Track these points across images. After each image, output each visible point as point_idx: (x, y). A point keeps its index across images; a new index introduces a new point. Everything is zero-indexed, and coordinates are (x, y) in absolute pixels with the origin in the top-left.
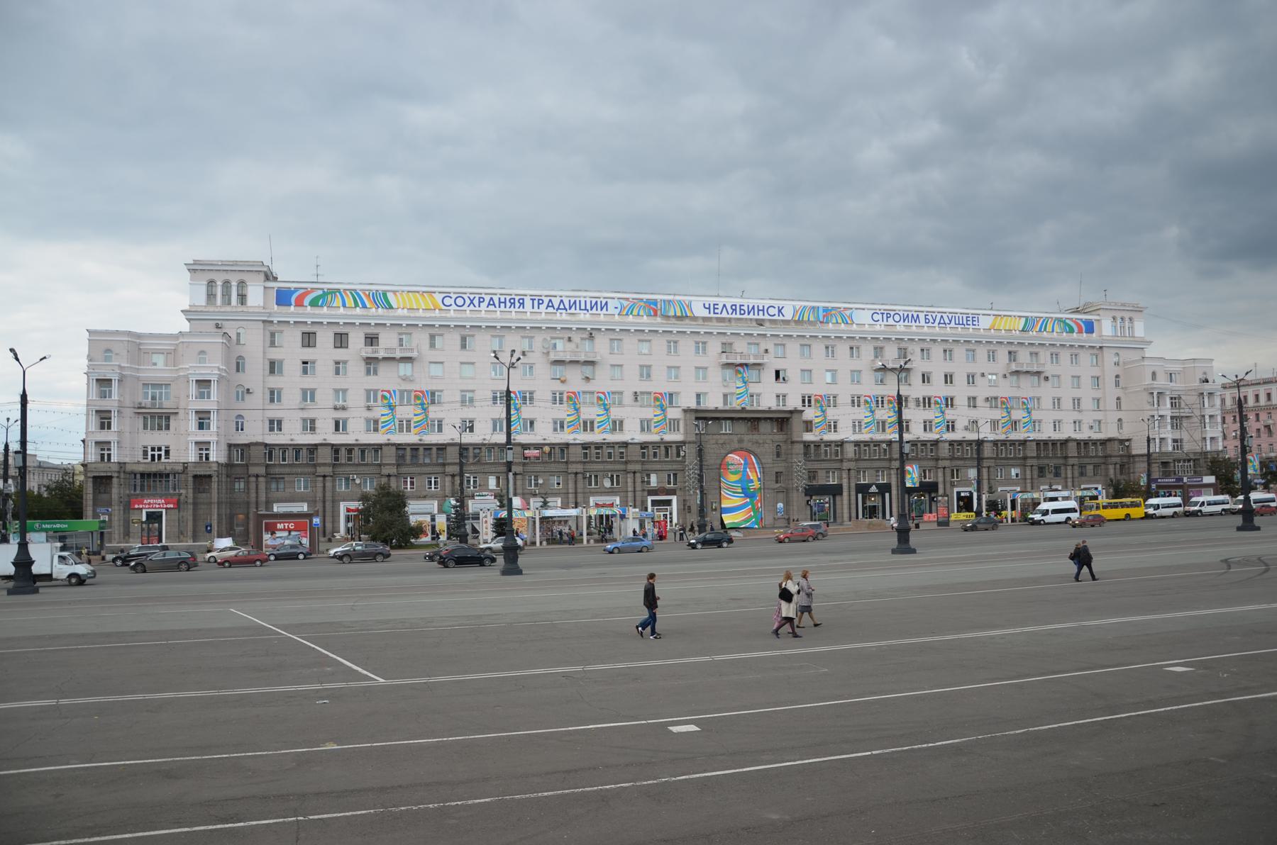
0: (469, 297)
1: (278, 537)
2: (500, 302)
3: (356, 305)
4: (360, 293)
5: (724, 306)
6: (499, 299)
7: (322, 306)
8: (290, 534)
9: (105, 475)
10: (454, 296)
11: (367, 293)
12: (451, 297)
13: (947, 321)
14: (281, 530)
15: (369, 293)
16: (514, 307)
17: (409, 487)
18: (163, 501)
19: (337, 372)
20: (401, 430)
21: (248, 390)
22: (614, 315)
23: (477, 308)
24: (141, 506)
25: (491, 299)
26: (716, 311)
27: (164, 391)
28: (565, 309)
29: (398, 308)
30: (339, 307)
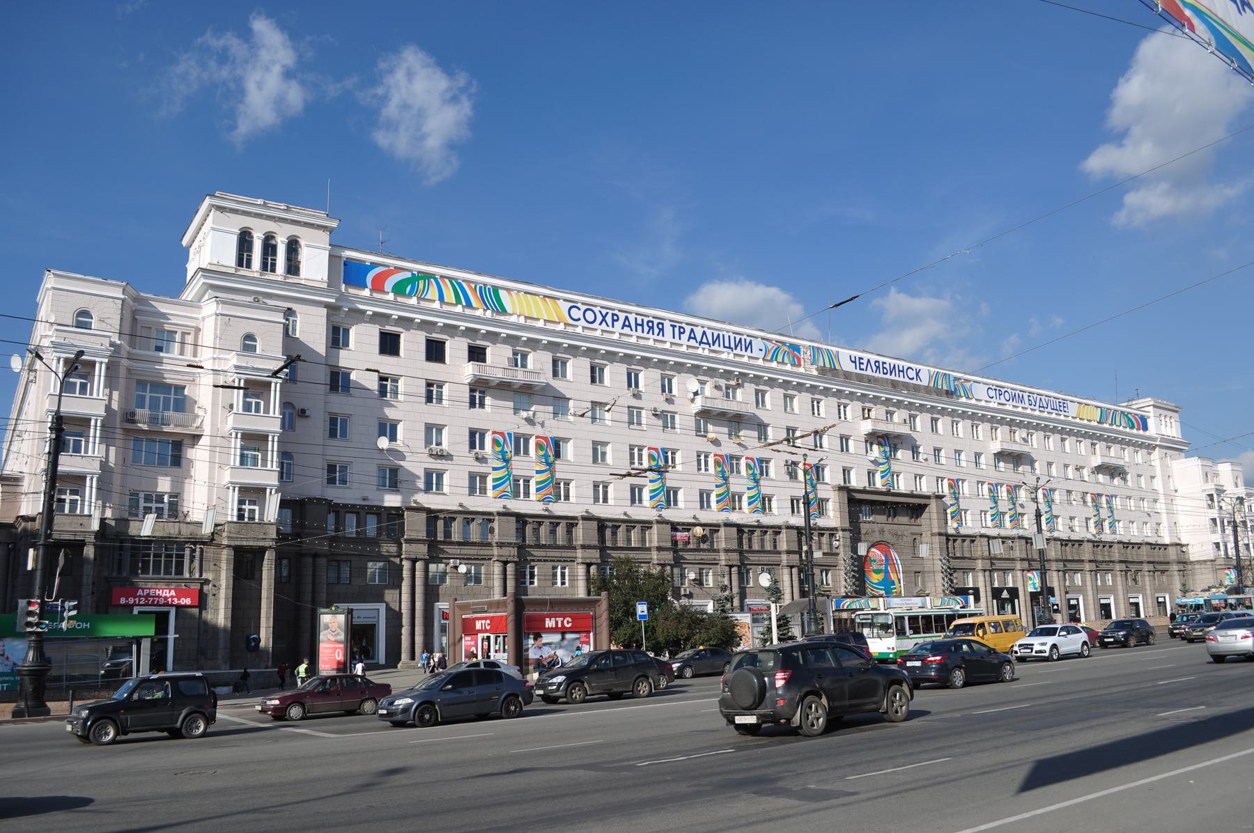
0: (600, 312)
1: (545, 644)
2: (637, 325)
3: (458, 302)
4: (464, 284)
5: (869, 361)
6: (636, 319)
7: (410, 296)
8: (563, 638)
9: (72, 538)
10: (583, 308)
11: (473, 286)
12: (579, 309)
13: (1045, 405)
14: (552, 631)
15: (476, 286)
16: (653, 334)
17: (559, 584)
18: (173, 593)
19: (429, 399)
20: (516, 494)
21: (303, 411)
22: (758, 359)
23: (610, 329)
24: (131, 601)
25: (627, 318)
26: (862, 366)
27: (172, 397)
28: (708, 343)
29: (513, 314)
30: (434, 301)
